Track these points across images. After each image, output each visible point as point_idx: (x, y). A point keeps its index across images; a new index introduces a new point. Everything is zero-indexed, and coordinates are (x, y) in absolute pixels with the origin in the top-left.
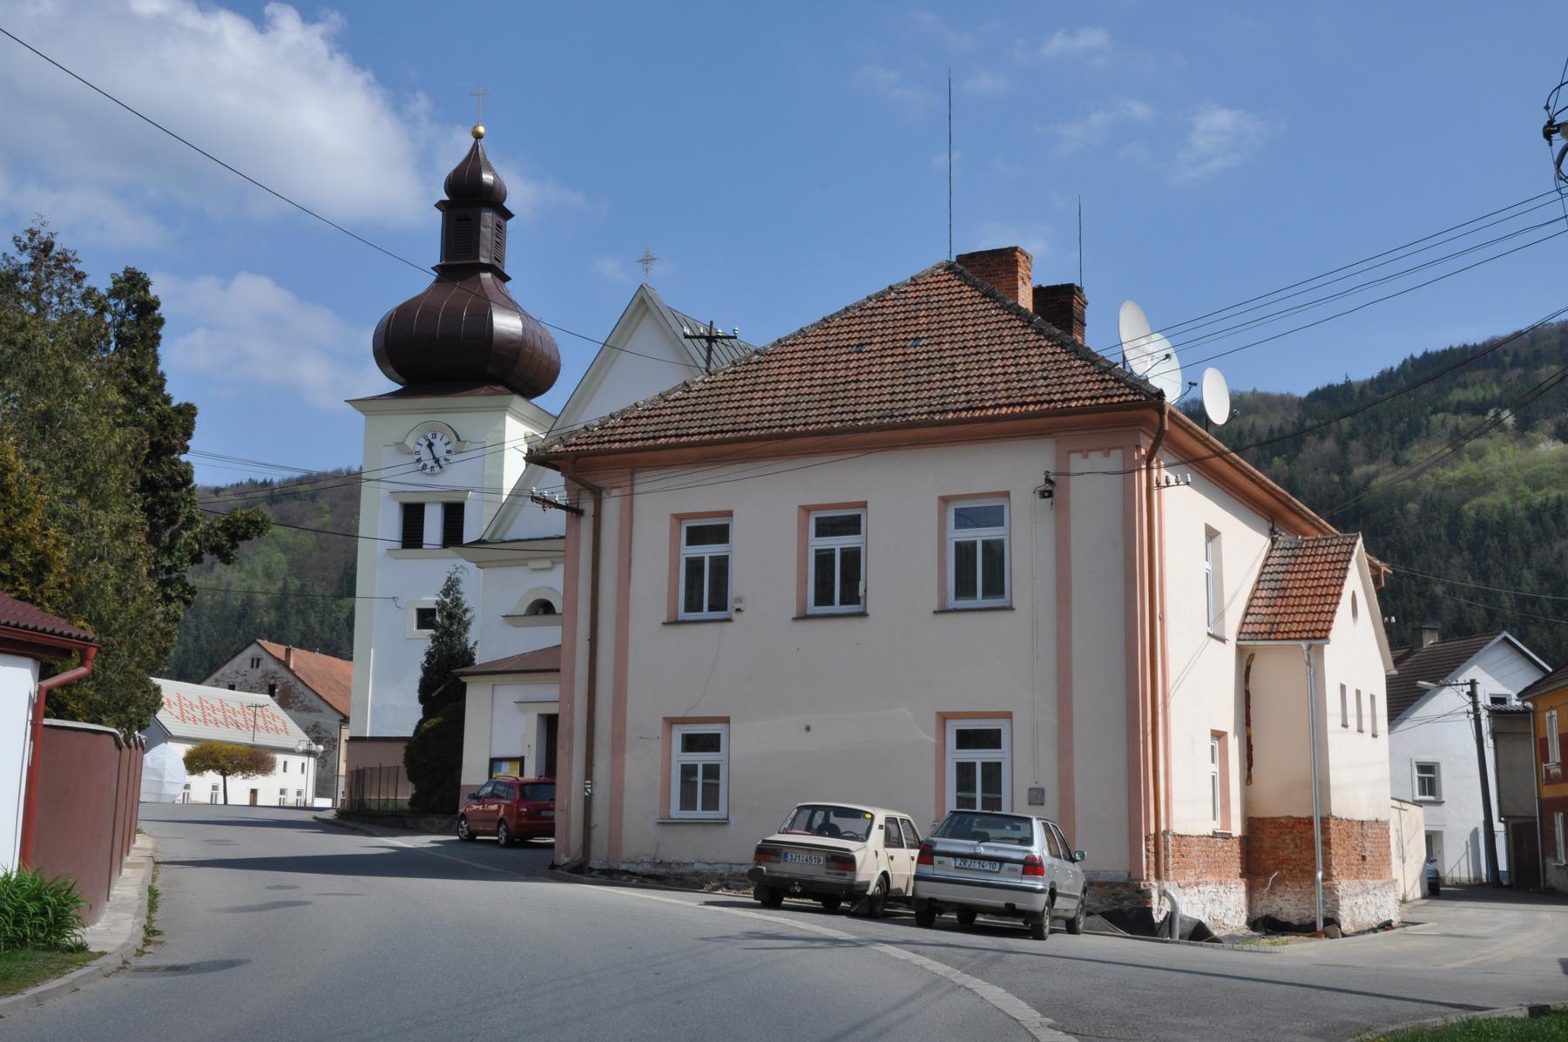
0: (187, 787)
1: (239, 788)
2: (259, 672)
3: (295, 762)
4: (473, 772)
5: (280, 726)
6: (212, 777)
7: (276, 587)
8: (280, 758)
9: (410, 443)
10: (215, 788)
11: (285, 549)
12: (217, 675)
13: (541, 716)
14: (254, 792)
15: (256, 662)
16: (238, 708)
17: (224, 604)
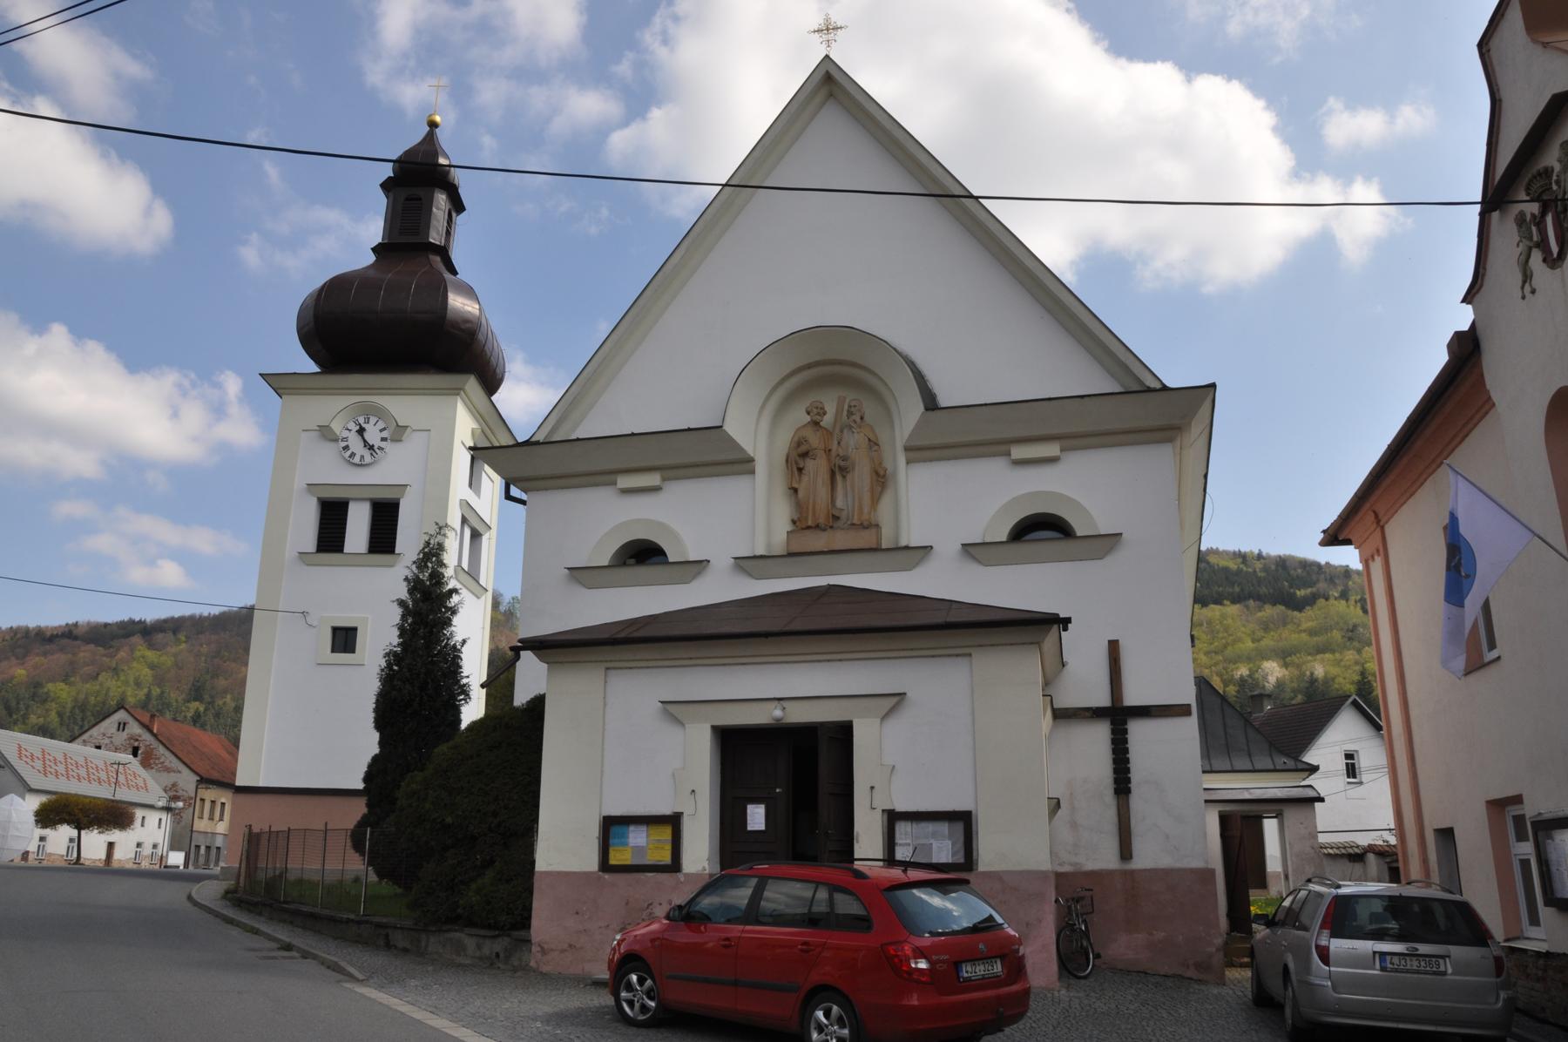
1: (94, 844)
2: (124, 735)
3: (153, 818)
4: (562, 842)
6: (65, 832)
7: (142, 694)
8: (139, 813)
9: (337, 427)
10: (71, 840)
11: (152, 667)
12: (85, 737)
13: (714, 728)
14: (111, 845)
15: (122, 726)
16: (101, 765)
17: (104, 703)
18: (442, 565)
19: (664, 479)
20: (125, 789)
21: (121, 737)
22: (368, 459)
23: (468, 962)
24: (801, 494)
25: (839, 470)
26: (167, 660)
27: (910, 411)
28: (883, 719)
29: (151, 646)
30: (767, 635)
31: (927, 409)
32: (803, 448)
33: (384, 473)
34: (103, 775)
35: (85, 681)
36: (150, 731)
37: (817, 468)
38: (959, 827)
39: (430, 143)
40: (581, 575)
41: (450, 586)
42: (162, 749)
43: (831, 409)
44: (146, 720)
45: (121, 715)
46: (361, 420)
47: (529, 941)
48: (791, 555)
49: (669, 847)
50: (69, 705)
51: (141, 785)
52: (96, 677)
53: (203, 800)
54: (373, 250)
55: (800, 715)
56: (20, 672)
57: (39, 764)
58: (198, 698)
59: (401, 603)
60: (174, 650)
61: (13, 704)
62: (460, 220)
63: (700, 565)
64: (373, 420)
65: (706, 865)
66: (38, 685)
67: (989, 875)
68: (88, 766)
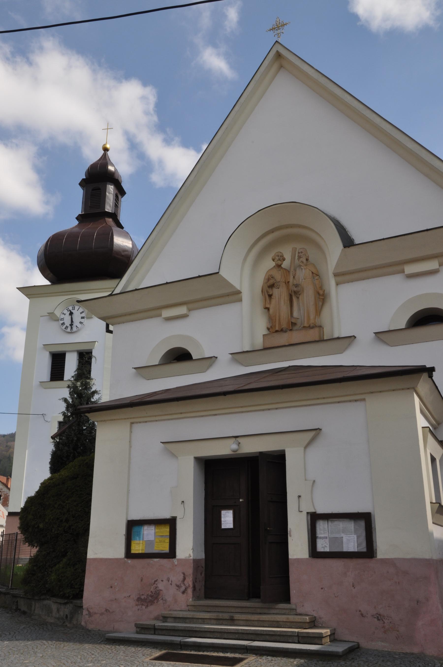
4: (104, 542)
9: (58, 313)
13: (197, 459)
19: (190, 310)
23: (52, 621)
24: (271, 311)
25: (294, 294)
27: (334, 247)
28: (306, 448)
30: (225, 394)
31: (345, 247)
32: (271, 282)
37: (281, 294)
38: (362, 524)
39: (104, 160)
40: (142, 371)
41: (93, 389)
43: (288, 256)
46: (71, 308)
47: (81, 607)
48: (265, 349)
49: (167, 540)
54: (77, 218)
55: (251, 447)
59: (65, 400)
62: (124, 200)
63: (212, 360)
65: (191, 552)
67: (384, 561)
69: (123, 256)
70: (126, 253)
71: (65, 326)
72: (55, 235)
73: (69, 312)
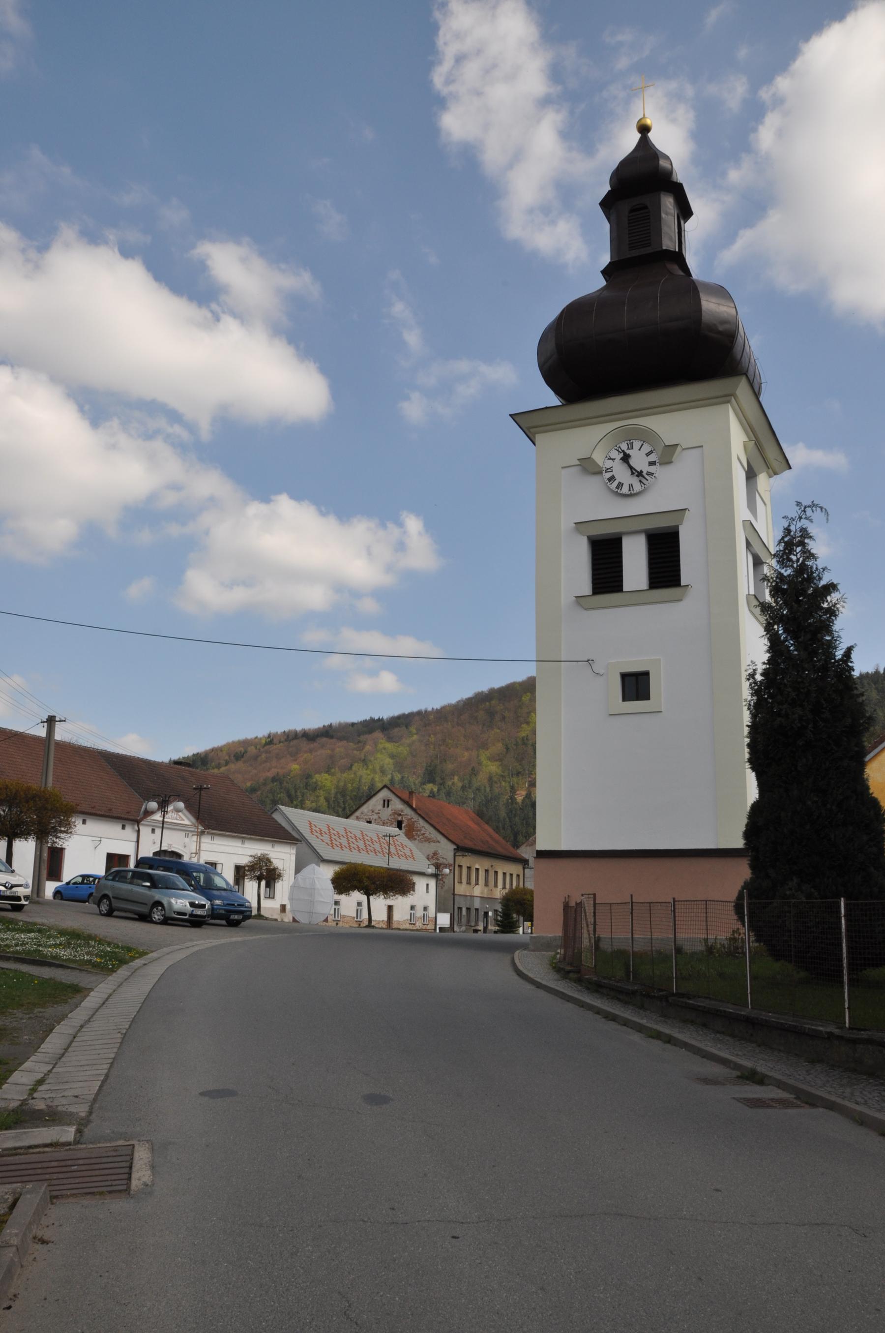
0: (337, 903)
5: (408, 853)
6: (357, 896)
9: (599, 457)
10: (359, 904)
11: (392, 756)
12: (358, 813)
14: (390, 908)
15: (386, 803)
16: (375, 838)
17: (359, 789)
18: (810, 555)
20: (396, 858)
21: (387, 813)
22: (637, 487)
26: (403, 750)
29: (390, 739)
33: (658, 500)
34: (377, 846)
35: (343, 771)
36: (411, 807)
41: (823, 583)
42: (421, 822)
44: (406, 796)
45: (385, 794)
46: (624, 446)
50: (333, 791)
51: (409, 855)
52: (350, 768)
53: (460, 866)
56: (295, 767)
57: (326, 838)
58: (432, 780)
60: (408, 741)
61: (293, 792)
64: (637, 444)
66: (309, 777)
68: (367, 837)
69: (720, 333)
70: (727, 326)
71: (615, 484)
72: (568, 306)
73: (622, 455)
